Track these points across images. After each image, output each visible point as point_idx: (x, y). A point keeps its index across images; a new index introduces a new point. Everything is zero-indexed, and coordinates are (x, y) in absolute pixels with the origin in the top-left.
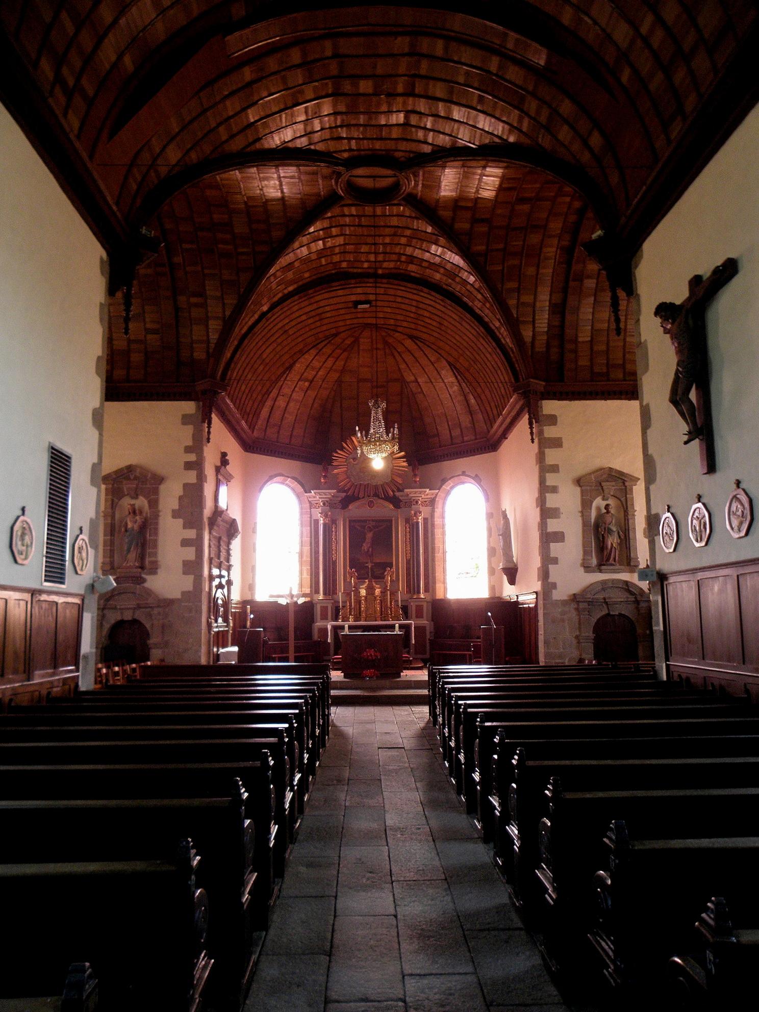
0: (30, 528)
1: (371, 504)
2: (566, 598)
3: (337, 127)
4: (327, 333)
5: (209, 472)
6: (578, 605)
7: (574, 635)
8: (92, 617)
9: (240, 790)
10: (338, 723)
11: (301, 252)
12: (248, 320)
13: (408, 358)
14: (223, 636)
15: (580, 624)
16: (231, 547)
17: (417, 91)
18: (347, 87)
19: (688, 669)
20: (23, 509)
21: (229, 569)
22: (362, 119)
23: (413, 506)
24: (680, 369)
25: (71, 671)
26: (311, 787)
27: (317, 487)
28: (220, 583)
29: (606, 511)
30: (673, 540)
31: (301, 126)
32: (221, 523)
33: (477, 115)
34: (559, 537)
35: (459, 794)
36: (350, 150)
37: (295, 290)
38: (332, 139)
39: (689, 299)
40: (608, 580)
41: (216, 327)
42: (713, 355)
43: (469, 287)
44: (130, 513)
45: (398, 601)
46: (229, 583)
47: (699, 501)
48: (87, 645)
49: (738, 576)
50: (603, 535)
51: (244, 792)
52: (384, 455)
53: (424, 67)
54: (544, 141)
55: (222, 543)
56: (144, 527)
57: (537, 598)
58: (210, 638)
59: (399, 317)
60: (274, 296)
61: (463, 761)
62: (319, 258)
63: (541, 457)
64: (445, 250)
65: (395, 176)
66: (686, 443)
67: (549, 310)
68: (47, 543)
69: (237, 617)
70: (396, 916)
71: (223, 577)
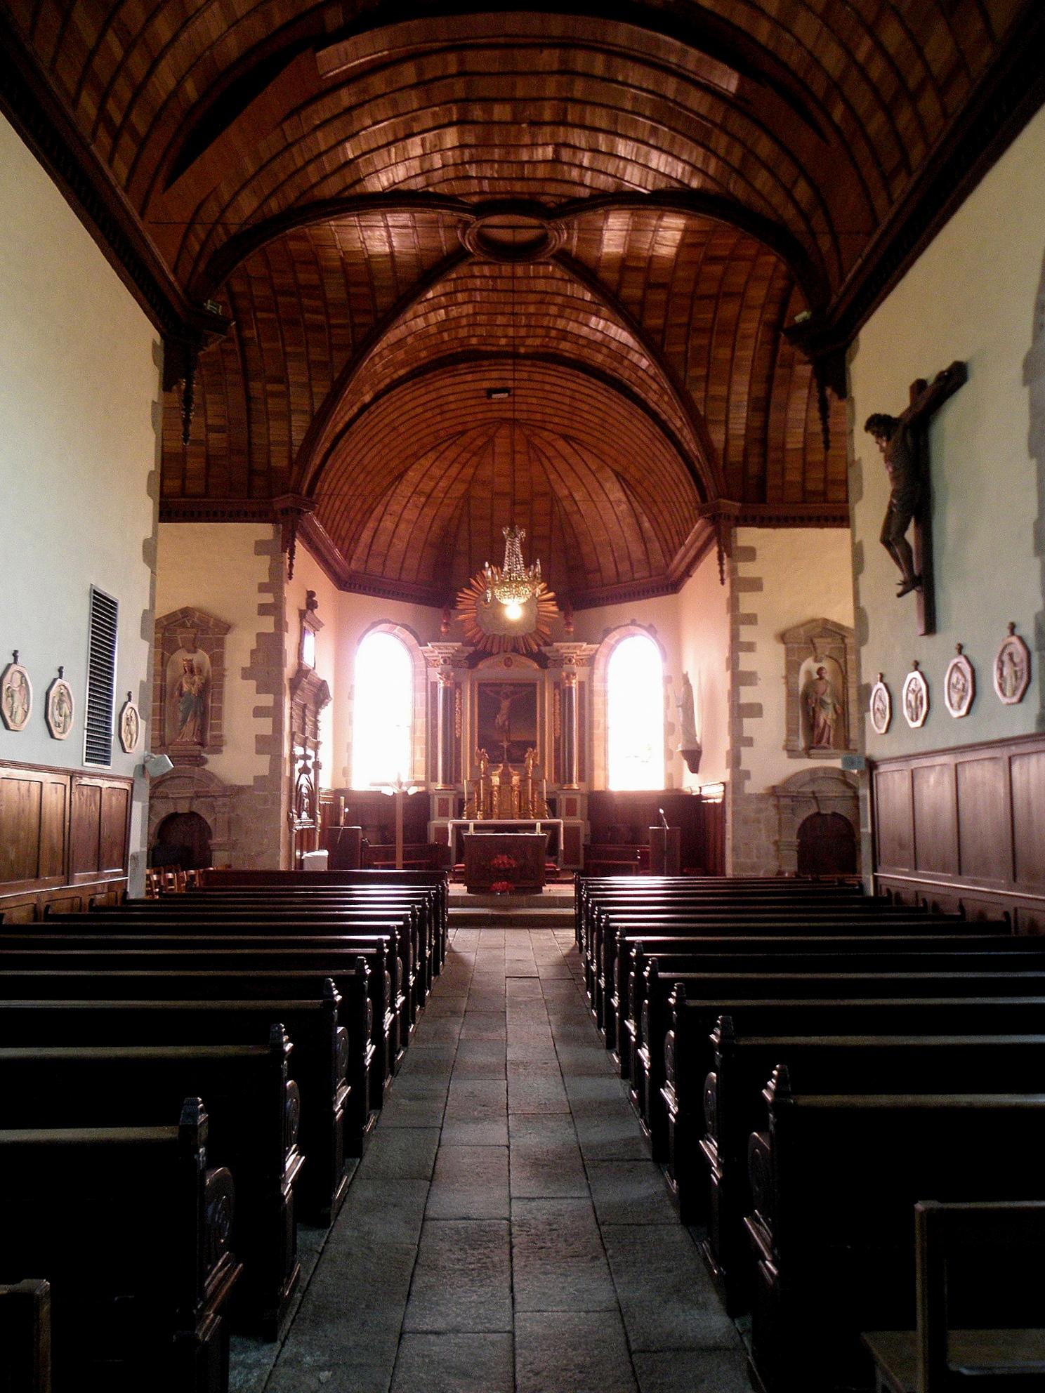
0: (68, 693)
1: (508, 663)
2: (762, 791)
3: (463, 163)
4: (452, 431)
5: (291, 617)
6: (779, 801)
7: (772, 841)
8: (143, 807)
9: (332, 991)
10: (456, 949)
11: (416, 322)
12: (343, 413)
13: (561, 466)
14: (309, 836)
15: (780, 825)
16: (319, 718)
17: (569, 118)
18: (477, 113)
19: (942, 888)
20: (60, 670)
21: (316, 747)
22: (497, 153)
23: (564, 666)
24: (895, 501)
25: (117, 875)
26: (418, 1020)
27: (436, 639)
28: (305, 765)
29: (818, 677)
30: (885, 718)
31: (416, 163)
32: (306, 686)
33: (649, 152)
34: (755, 710)
35: (599, 1028)
36: (482, 193)
37: (407, 373)
38: (457, 178)
39: (909, 409)
40: (818, 768)
41: (301, 424)
42: (937, 484)
43: (640, 373)
44: (186, 672)
45: (542, 793)
46: (317, 765)
47: (916, 669)
48: (137, 844)
49: (956, 765)
50: (813, 708)
51: (338, 994)
52: (523, 600)
53: (579, 89)
54: (737, 188)
55: (307, 712)
56: (204, 690)
57: (724, 791)
58: (291, 838)
59: (548, 411)
60: (379, 383)
61: (603, 985)
62: (440, 332)
63: (733, 604)
64: (609, 323)
65: (541, 227)
66: (900, 595)
67: (748, 406)
68: (89, 712)
69: (327, 811)
70: (508, 1147)
71: (308, 757)
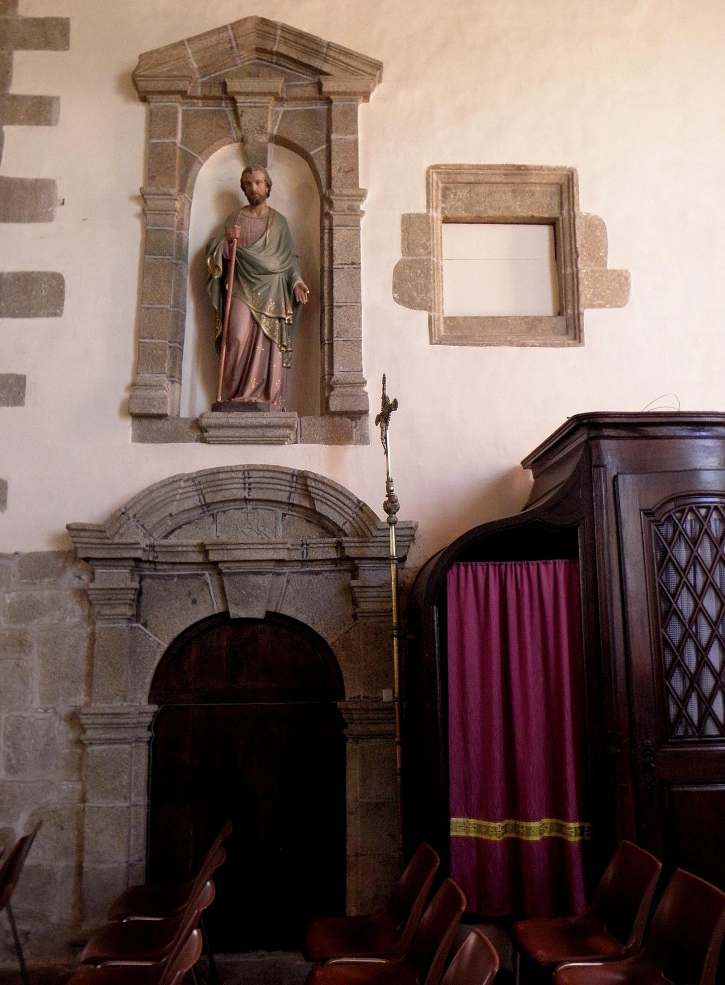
7: (64, 710)
